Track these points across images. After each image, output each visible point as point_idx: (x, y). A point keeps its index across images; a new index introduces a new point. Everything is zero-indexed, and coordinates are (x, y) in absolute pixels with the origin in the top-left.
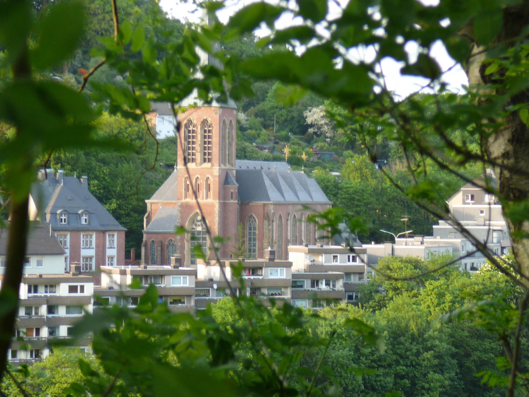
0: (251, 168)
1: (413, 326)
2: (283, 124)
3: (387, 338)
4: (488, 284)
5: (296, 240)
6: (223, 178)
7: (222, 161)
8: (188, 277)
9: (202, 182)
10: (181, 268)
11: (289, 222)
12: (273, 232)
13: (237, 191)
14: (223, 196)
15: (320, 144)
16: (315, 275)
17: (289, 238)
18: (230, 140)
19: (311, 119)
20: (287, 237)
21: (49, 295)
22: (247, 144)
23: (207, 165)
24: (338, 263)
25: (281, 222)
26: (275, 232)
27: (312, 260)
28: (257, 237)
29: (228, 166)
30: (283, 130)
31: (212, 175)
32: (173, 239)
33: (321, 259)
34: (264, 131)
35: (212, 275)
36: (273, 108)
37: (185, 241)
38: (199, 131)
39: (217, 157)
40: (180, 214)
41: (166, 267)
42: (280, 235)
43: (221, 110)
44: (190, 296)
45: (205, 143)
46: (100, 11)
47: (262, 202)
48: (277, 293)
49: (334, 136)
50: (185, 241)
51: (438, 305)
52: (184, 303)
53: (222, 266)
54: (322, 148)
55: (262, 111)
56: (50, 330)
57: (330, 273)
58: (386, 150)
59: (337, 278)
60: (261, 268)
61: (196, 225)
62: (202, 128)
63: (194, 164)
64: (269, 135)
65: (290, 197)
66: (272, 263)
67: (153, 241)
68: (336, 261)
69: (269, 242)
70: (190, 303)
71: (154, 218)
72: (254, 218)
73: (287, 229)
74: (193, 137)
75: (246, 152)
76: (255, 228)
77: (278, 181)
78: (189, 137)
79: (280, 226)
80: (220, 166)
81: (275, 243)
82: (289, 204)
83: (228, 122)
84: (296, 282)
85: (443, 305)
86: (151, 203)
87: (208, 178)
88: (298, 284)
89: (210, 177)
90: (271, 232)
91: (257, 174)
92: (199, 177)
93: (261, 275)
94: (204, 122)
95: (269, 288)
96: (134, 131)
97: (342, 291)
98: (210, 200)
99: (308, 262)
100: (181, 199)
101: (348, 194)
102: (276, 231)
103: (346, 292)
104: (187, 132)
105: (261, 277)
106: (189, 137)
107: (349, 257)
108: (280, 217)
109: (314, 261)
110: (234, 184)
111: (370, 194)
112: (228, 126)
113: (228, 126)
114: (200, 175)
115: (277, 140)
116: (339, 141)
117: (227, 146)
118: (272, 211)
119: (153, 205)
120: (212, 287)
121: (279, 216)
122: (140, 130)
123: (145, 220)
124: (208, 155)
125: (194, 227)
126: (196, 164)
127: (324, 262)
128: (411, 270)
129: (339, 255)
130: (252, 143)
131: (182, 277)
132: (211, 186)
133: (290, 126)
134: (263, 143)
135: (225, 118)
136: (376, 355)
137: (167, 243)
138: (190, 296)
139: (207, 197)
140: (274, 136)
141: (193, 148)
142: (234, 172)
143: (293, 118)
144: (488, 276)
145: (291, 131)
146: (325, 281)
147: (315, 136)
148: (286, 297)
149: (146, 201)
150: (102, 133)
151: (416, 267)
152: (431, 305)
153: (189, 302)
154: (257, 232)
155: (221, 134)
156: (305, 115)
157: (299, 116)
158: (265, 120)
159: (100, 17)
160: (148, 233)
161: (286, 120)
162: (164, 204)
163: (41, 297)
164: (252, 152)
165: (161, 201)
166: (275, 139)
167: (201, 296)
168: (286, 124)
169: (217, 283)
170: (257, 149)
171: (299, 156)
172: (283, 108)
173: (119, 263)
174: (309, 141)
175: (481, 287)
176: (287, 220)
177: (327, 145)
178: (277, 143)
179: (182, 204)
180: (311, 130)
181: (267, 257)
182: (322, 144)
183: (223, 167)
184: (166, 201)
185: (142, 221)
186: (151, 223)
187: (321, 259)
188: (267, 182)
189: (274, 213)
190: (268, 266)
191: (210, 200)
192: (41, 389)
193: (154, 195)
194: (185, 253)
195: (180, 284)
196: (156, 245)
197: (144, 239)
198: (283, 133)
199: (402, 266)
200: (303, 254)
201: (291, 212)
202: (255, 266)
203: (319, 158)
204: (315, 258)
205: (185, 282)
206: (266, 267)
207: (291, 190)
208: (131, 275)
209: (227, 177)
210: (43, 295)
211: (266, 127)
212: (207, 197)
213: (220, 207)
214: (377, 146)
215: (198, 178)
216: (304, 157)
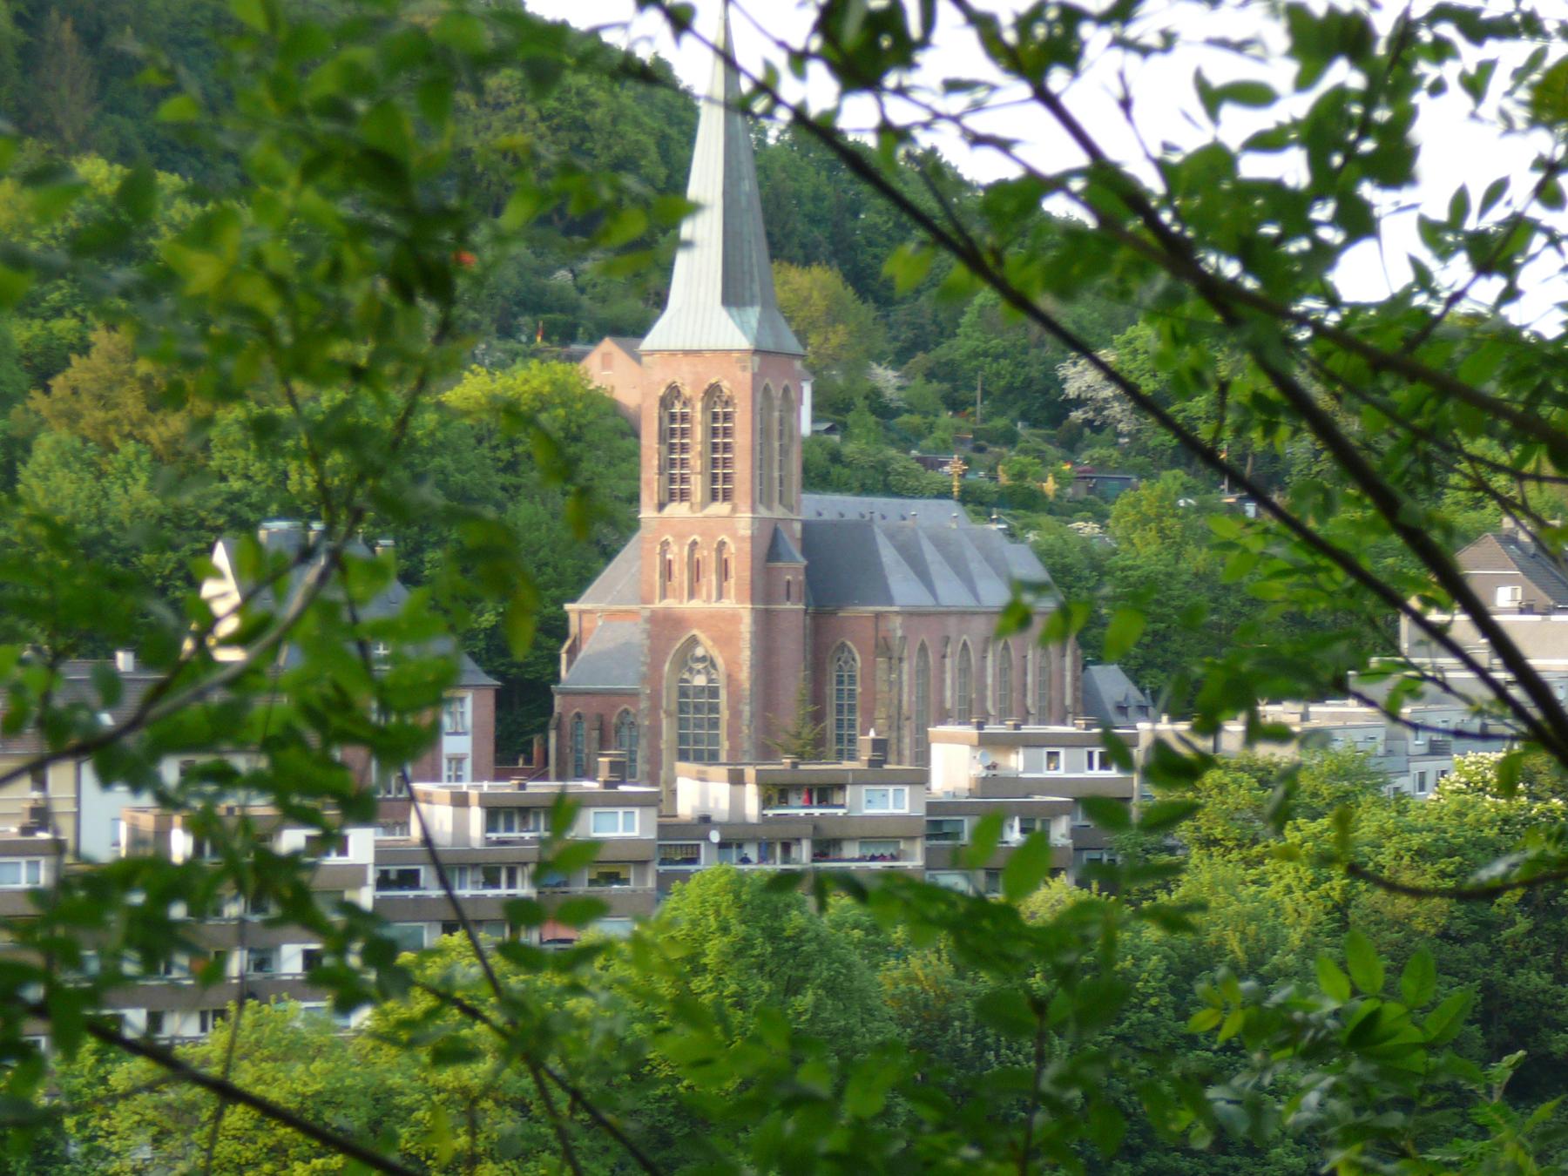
0: (852, 516)
1: (1234, 943)
2: (1004, 398)
3: (1160, 975)
4: (1451, 826)
5: (1050, 709)
6: (765, 544)
7: (762, 496)
8: (637, 811)
9: (706, 554)
10: (622, 788)
11: (948, 661)
12: (901, 689)
13: (801, 578)
14: (764, 590)
15: (1097, 452)
16: (993, 801)
17: (948, 705)
18: (786, 440)
19: (1077, 385)
20: (942, 701)
21: (817, 812)
22: (892, 452)
23: (720, 508)
24: (1061, 773)
25: (926, 662)
26: (906, 689)
27: (989, 763)
28: (858, 702)
29: (779, 512)
30: (1002, 414)
31: (734, 536)
32: (632, 710)
33: (1016, 762)
34: (946, 417)
35: (711, 805)
36: (974, 355)
37: (663, 715)
38: (698, 416)
39: (748, 486)
40: (647, 642)
41: (589, 785)
42: (924, 699)
43: (757, 359)
44: (643, 863)
45: (715, 447)
46: (510, 97)
47: (871, 608)
48: (887, 853)
49: (1139, 431)
50: (663, 715)
51: (1315, 884)
52: (626, 881)
53: (737, 779)
54: (1102, 464)
55: (946, 364)
56: (253, 957)
57: (1037, 798)
58: (1279, 467)
59: (1054, 811)
60: (841, 787)
61: (691, 670)
62: (705, 409)
63: (686, 505)
64: (958, 429)
65: (951, 593)
66: (878, 773)
67: (578, 715)
68: (1056, 768)
69: (889, 717)
70: (644, 882)
71: (585, 650)
72: (850, 651)
73: (943, 681)
74: (684, 433)
75: (888, 473)
76: (852, 678)
77: (921, 550)
78: (672, 432)
79: (922, 672)
80: (753, 510)
81: (908, 719)
82: (948, 614)
83: (777, 393)
84: (939, 823)
85: (1327, 886)
86: (581, 613)
87: (722, 544)
88: (946, 829)
89: (727, 540)
90: (895, 690)
91: (861, 531)
92: (699, 539)
93: (842, 806)
94: (713, 392)
95: (864, 840)
96: (555, 419)
97: (1064, 848)
98: (729, 604)
99: (978, 770)
100: (651, 601)
101: (1129, 585)
102: (910, 686)
103: (1078, 850)
104: (666, 419)
105: (840, 812)
106: (672, 432)
107: (1090, 755)
108: (923, 649)
109: (994, 766)
110: (793, 559)
111: (1187, 583)
112: (777, 403)
113: (777, 403)
114: (701, 535)
115: (982, 443)
116: (1151, 444)
117: (777, 457)
118: (899, 633)
119: (585, 617)
120: (707, 839)
121: (918, 645)
122: (573, 418)
123: (564, 657)
124: (725, 482)
125: (686, 676)
126: (692, 505)
127: (1021, 769)
128: (1250, 790)
129: (1062, 752)
130: (907, 451)
131: (621, 811)
132: (676, 568)
133: (1022, 405)
134: (937, 450)
135: (767, 380)
136: (1127, 1023)
137: (614, 720)
138: (643, 863)
139: (720, 596)
140: (974, 432)
141: (684, 463)
142: (798, 527)
143: (1029, 382)
144: (1453, 807)
145: (1024, 416)
146: (1021, 821)
147: (1087, 431)
148: (909, 864)
149: (568, 606)
150: (1393, 442)
151: (1263, 784)
152: (1294, 884)
153: (642, 878)
154: (859, 690)
155: (758, 426)
156: (1061, 373)
157: (1046, 375)
158: (956, 390)
159: (512, 112)
160: (566, 693)
161: (1010, 389)
162: (611, 615)
163: (796, 818)
164: (906, 475)
165: (603, 606)
166: (975, 439)
167: (678, 863)
168: (1010, 397)
169: (720, 826)
170: (917, 465)
171: (1034, 485)
172: (1005, 355)
173: (478, 776)
174: (1071, 444)
175: (1428, 838)
176: (944, 657)
177: (1115, 454)
178: (981, 450)
179: (653, 612)
180: (1077, 415)
181: (865, 754)
182: (1104, 452)
183: (763, 512)
184: (615, 607)
185: (557, 660)
186: (575, 664)
187: (1016, 762)
188: (888, 555)
189: (904, 638)
190: (860, 779)
191: (729, 604)
192: (197, 1118)
193: (589, 591)
194: (663, 746)
195: (633, 829)
196: (585, 725)
197: (557, 709)
198: (1000, 423)
199: (1227, 780)
200: (965, 750)
201: (953, 635)
202: (825, 780)
203: (1090, 490)
204: (998, 759)
205: (628, 826)
206: (853, 784)
207: (958, 574)
208: (481, 805)
209: (775, 538)
210: (802, 812)
211: (956, 405)
212: (720, 596)
213: (756, 621)
214: (1255, 456)
215: (694, 543)
216: (1050, 486)
